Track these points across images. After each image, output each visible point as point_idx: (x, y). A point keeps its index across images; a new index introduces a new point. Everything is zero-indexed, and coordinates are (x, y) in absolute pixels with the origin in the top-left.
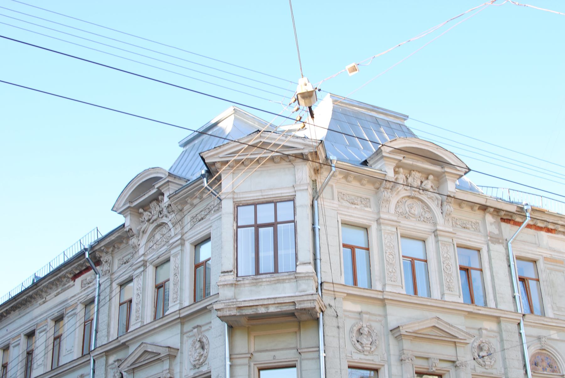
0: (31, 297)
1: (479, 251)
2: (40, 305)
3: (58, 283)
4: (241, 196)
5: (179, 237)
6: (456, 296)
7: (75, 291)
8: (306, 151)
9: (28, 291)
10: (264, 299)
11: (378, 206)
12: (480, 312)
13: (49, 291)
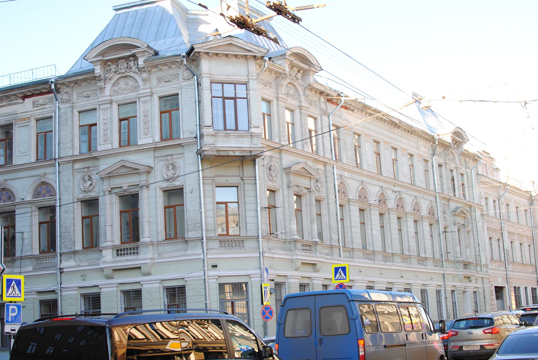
5: (149, 90)
8: (259, 55)
11: (277, 89)
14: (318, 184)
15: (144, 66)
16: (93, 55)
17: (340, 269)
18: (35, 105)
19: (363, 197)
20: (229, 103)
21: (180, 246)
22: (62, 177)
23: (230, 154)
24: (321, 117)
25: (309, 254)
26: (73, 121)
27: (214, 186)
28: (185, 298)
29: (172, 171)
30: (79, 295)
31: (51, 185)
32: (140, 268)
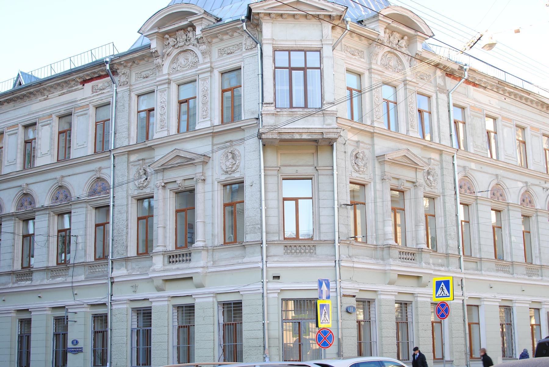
0: (31, 93)
1: (429, 97)
2: (40, 101)
3: (65, 85)
4: (279, 43)
5: (209, 65)
6: (416, 134)
7: (85, 93)
8: (334, 14)
9: (29, 88)
10: (300, 128)
11: (370, 59)
12: (432, 146)
13: (52, 90)
14: (430, 177)
15: (201, 36)
16: (149, 28)
17: (443, 284)
18: (94, 90)
19: (498, 194)
20: (298, 76)
21: (238, 252)
22: (116, 172)
23: (296, 138)
24: (437, 95)
25: (410, 264)
26: (129, 107)
27: (280, 178)
28: (241, 317)
29: (231, 160)
30: (130, 310)
31: (107, 181)
32: (191, 278)
